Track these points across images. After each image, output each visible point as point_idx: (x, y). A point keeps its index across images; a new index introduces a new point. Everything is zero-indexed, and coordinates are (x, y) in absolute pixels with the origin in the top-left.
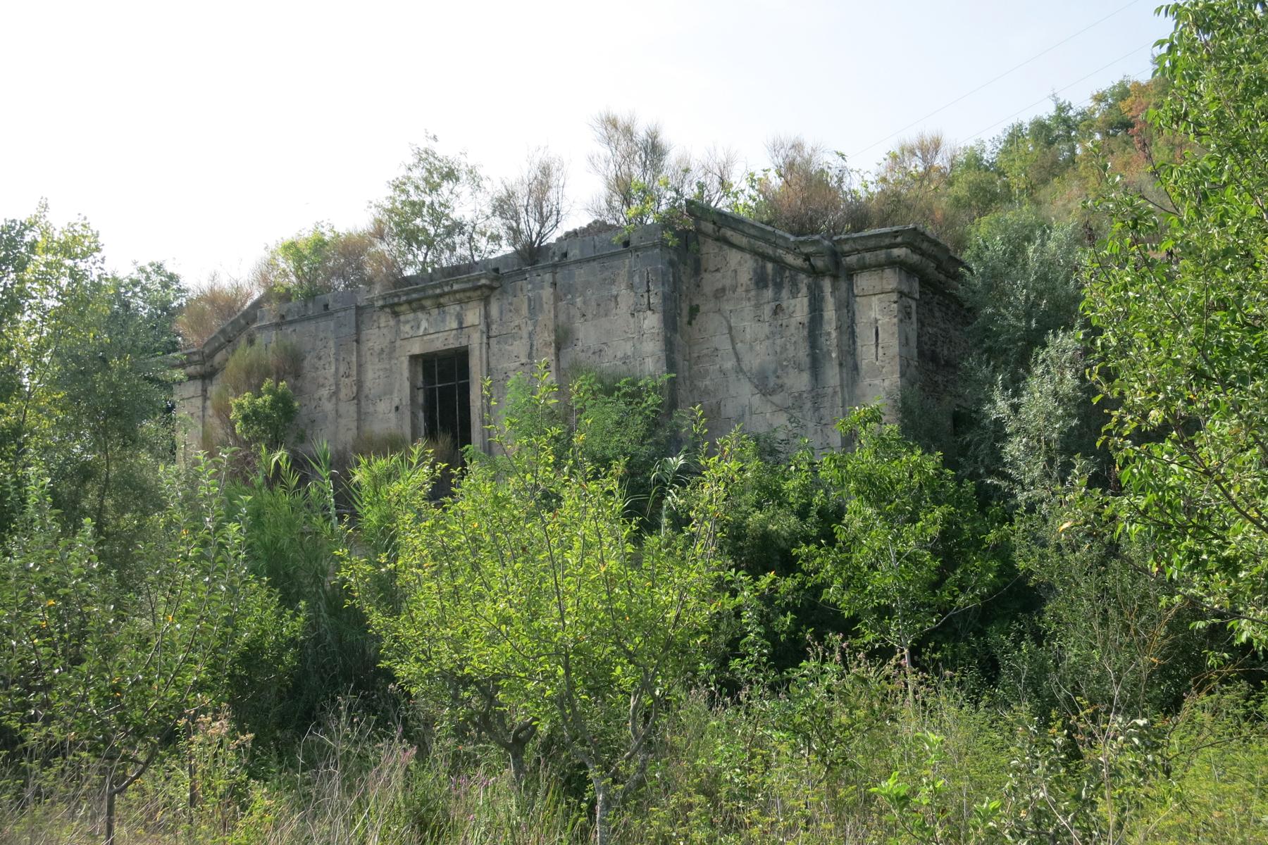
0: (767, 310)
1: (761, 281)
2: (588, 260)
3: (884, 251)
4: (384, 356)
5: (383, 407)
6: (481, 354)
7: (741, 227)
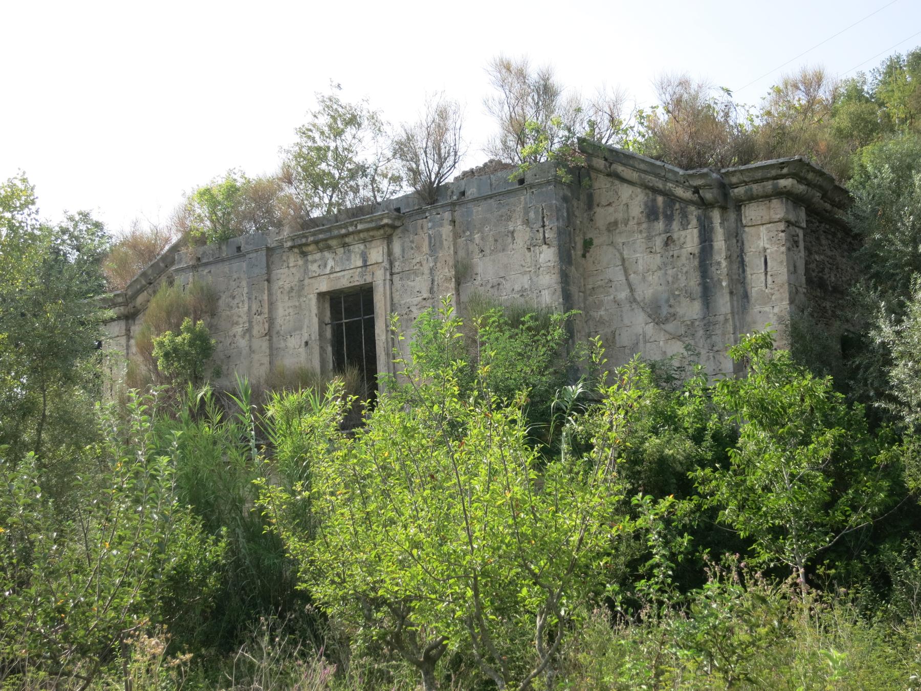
0: (659, 242)
1: (652, 214)
2: (486, 198)
3: (770, 182)
4: (293, 294)
5: (294, 342)
7: (631, 162)
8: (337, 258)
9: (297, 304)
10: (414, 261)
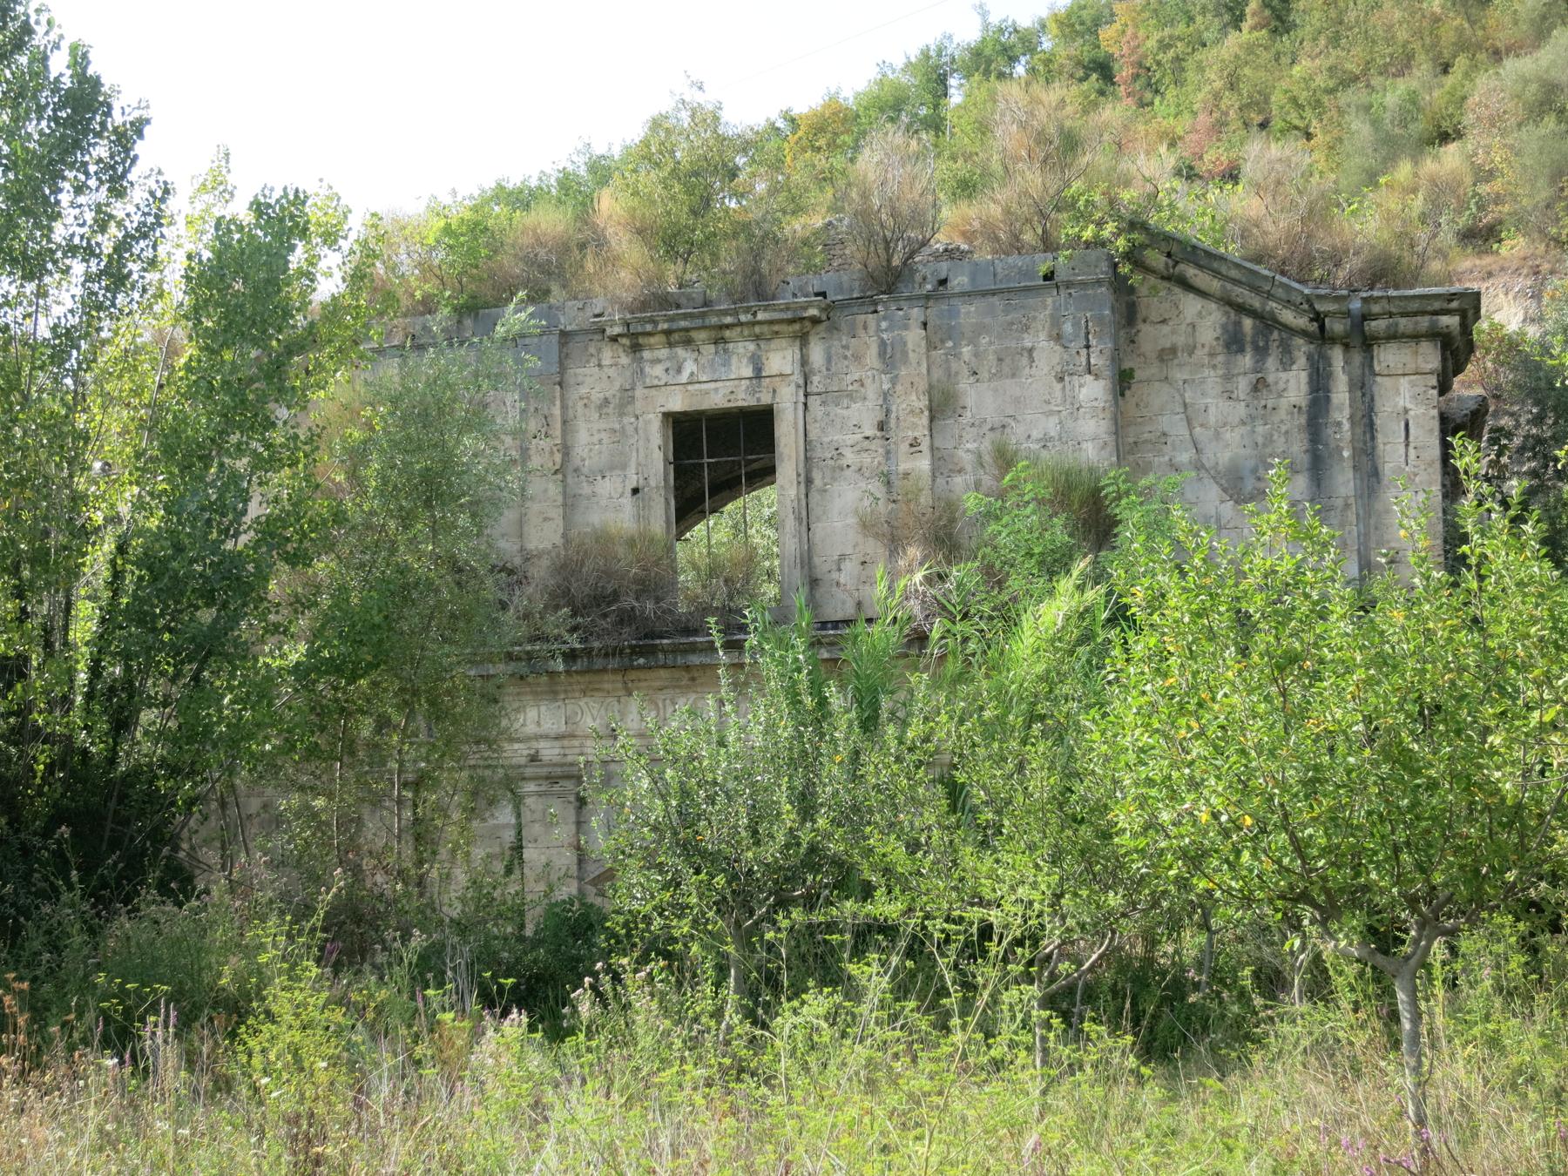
0: (1243, 385)
1: (1233, 342)
2: (985, 294)
3: (1427, 318)
4: (610, 410)
5: (611, 489)
6: (796, 418)
7: (1215, 265)
8: (703, 360)
9: (617, 426)
10: (849, 378)
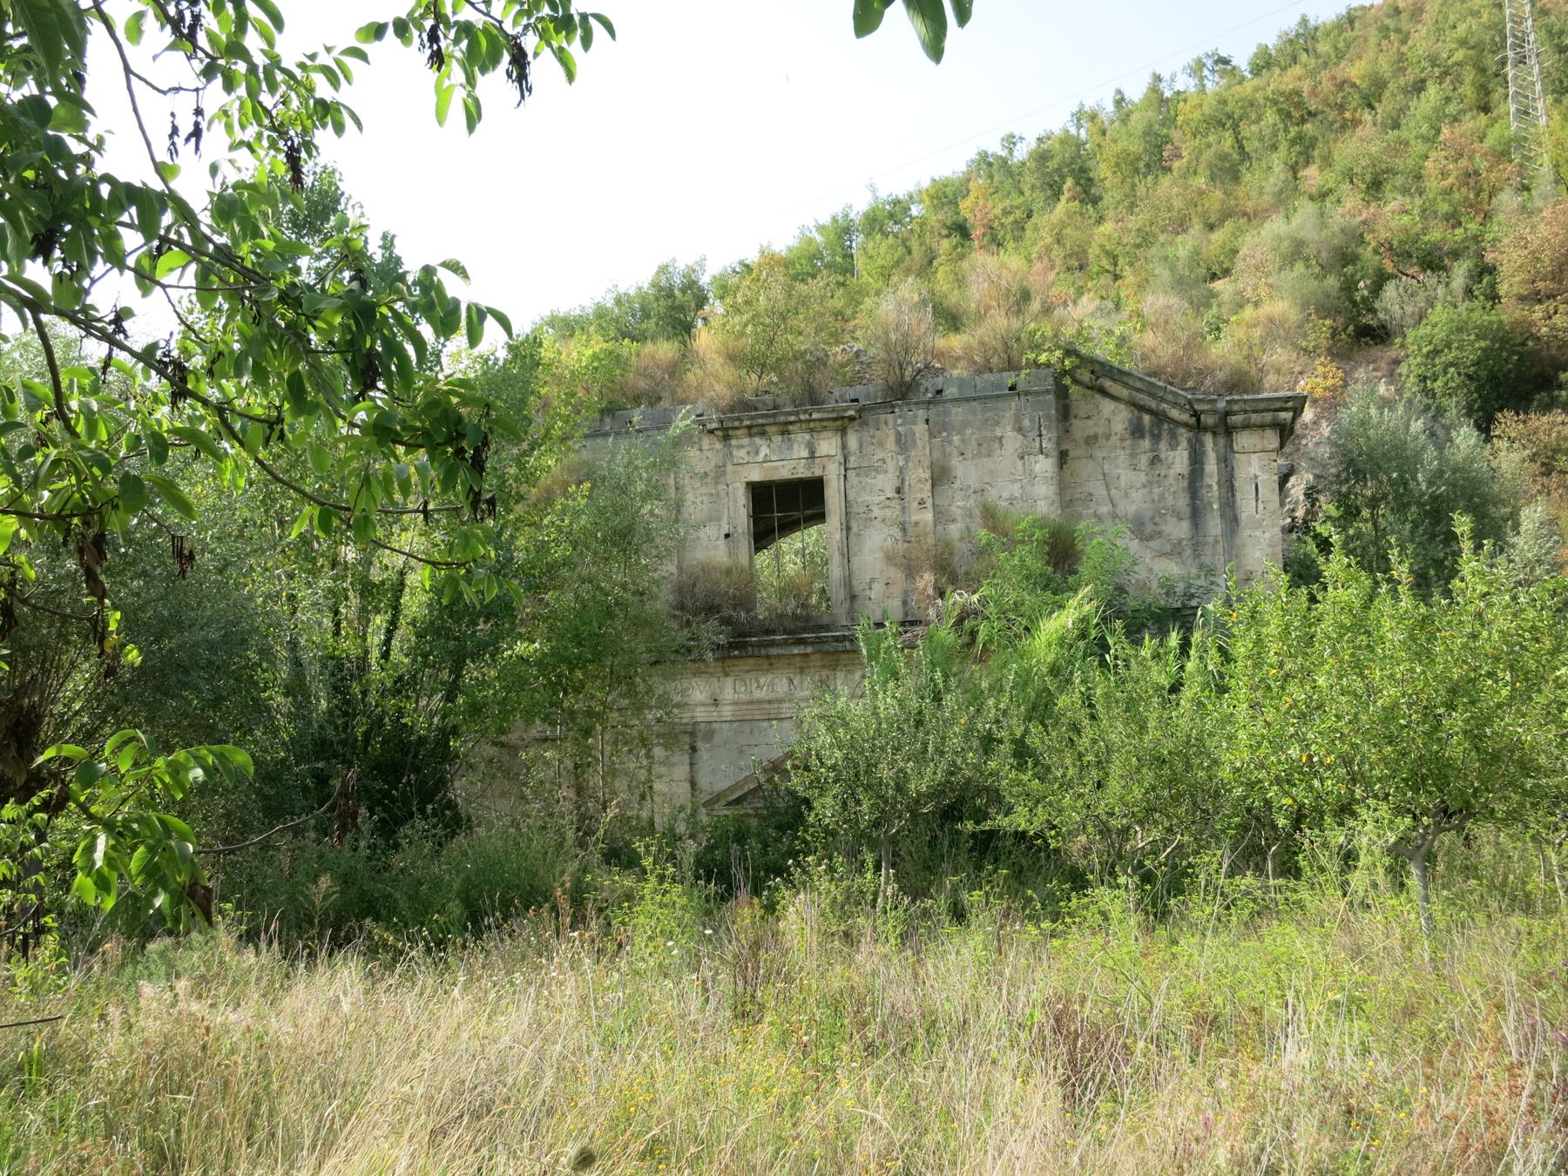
0: (1144, 460)
1: (1137, 431)
2: (968, 400)
4: (708, 480)
